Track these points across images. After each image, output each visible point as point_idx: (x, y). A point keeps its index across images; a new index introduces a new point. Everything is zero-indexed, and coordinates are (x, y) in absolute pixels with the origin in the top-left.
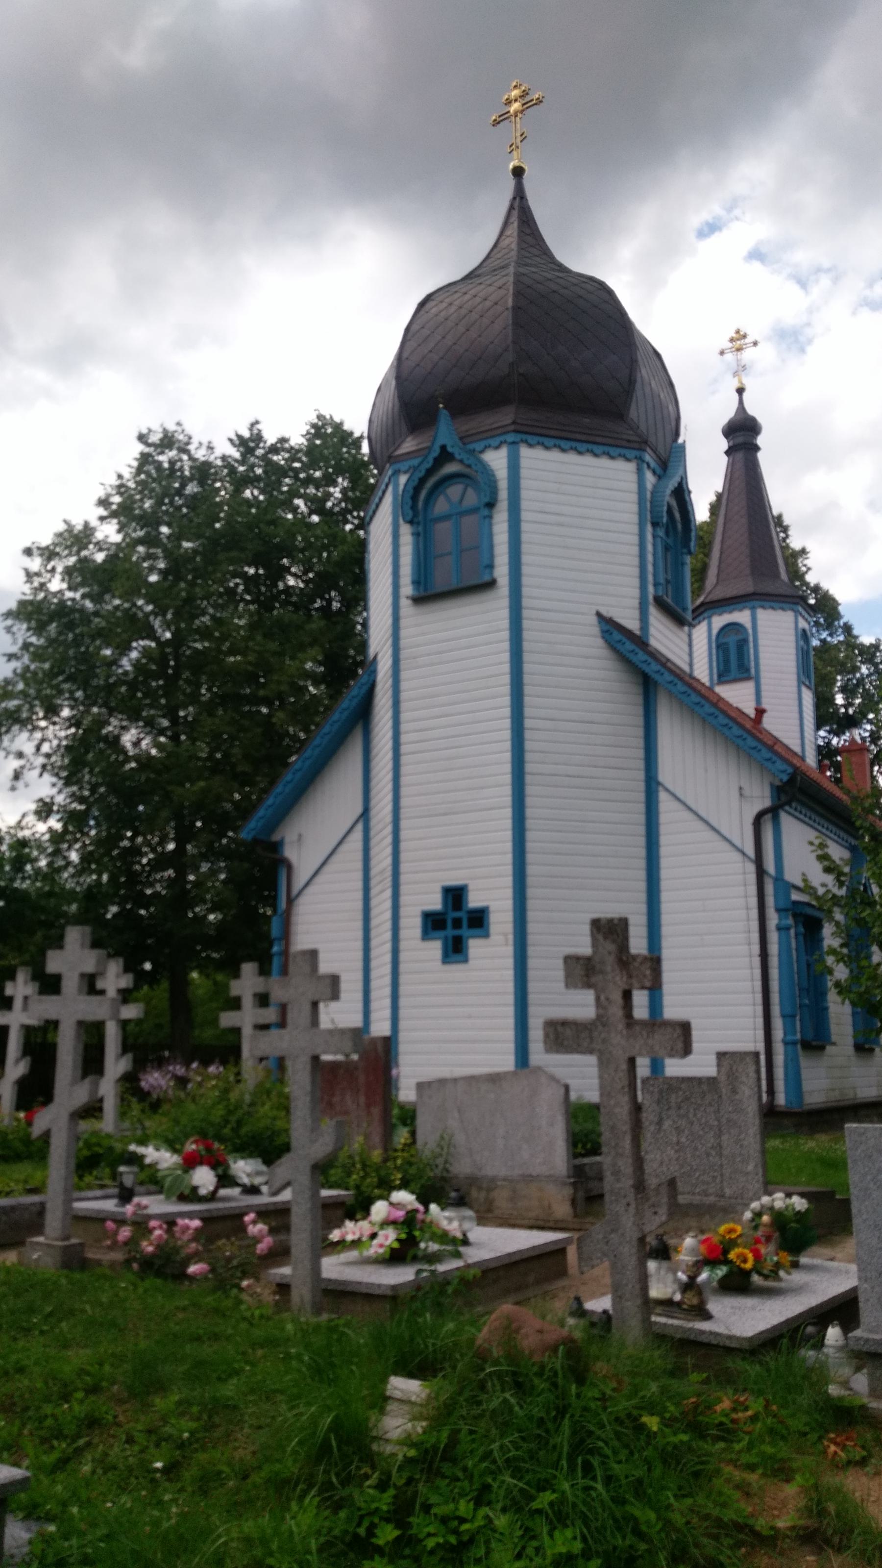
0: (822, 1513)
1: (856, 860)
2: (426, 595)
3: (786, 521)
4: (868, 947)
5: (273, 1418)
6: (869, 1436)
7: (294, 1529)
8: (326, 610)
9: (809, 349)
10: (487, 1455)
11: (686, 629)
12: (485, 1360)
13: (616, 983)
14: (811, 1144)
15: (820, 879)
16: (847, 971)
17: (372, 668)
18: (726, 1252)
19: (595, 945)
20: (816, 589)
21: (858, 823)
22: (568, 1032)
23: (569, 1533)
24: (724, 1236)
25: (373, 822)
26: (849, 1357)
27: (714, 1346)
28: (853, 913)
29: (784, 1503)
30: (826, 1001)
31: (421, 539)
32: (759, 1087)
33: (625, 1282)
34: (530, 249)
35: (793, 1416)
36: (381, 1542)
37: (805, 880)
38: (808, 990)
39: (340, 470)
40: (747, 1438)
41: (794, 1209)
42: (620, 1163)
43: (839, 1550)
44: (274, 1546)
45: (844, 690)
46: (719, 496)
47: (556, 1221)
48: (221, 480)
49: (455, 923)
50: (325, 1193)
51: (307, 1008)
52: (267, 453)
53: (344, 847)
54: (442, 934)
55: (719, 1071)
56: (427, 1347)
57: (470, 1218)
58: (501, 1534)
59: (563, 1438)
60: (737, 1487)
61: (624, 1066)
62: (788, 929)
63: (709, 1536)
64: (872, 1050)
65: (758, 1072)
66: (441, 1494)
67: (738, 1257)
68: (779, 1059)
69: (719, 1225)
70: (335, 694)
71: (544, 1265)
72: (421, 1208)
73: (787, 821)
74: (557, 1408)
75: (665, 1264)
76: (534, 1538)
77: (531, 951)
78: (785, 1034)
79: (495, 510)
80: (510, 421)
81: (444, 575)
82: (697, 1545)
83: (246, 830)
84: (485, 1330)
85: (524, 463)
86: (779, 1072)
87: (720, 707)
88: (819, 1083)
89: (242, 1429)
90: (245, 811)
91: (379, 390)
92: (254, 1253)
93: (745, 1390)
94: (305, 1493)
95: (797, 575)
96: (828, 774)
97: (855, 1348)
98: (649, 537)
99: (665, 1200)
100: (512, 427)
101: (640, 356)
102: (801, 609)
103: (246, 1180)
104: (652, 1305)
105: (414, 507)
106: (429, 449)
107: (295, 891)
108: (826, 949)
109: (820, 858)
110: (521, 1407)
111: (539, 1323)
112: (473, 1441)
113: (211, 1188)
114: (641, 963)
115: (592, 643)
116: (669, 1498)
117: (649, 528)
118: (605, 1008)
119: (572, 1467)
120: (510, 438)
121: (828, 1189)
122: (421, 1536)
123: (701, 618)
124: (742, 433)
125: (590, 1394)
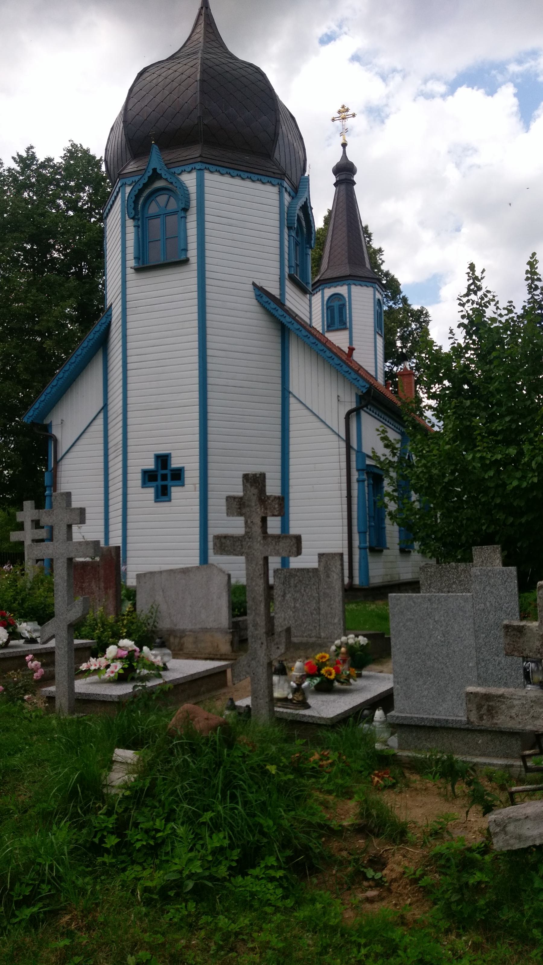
2: (143, 267)
3: (370, 230)
4: (410, 491)
5: (43, 776)
6: (397, 771)
7: (54, 841)
8: (78, 274)
9: (386, 121)
10: (174, 792)
11: (308, 295)
12: (173, 737)
13: (257, 512)
14: (373, 607)
15: (382, 452)
16: (396, 506)
17: (108, 313)
18: (319, 669)
19: (244, 490)
20: (387, 274)
21: (405, 418)
22: (228, 542)
23: (221, 835)
25: (110, 413)
26: (387, 727)
27: (310, 723)
28: (400, 471)
29: (348, 812)
31: (140, 230)
32: (343, 573)
33: (259, 688)
35: (355, 762)
36: (108, 846)
37: (373, 452)
39: (87, 182)
40: (328, 775)
41: (360, 644)
42: (258, 619)
44: (42, 851)
45: (402, 338)
46: (330, 212)
47: (221, 655)
48: (7, 185)
49: (163, 477)
50: (76, 642)
51: (64, 529)
53: (91, 429)
54: (154, 484)
55: (319, 565)
56: (138, 731)
57: (168, 654)
58: (181, 837)
59: (219, 780)
60: (321, 804)
61: (261, 562)
62: (363, 481)
63: (304, 832)
64: (410, 552)
65: (342, 565)
66: (145, 816)
67: (326, 672)
69: (316, 654)
71: (212, 681)
72: (138, 649)
73: (365, 417)
75: (283, 678)
76: (201, 839)
77: (210, 494)
78: (360, 543)
79: (188, 213)
80: (198, 155)
82: (296, 838)
83: (27, 416)
84: (174, 719)
85: (207, 183)
86: (356, 565)
87: (328, 346)
88: (379, 571)
89: (23, 783)
90: (26, 404)
91: (112, 129)
92: (32, 678)
93: (327, 748)
95: (376, 265)
96: (391, 389)
98: (286, 236)
99: (284, 640)
101: (282, 118)
102: (377, 287)
103: (27, 635)
105: (135, 208)
107: (59, 456)
108: (385, 492)
109: (383, 439)
110: (194, 764)
111: (207, 715)
112: (165, 784)
113: (5, 640)
114: (272, 501)
116: (281, 812)
117: (286, 230)
118: (251, 528)
120: (198, 166)
121: (381, 632)
122: (132, 842)
123: (318, 290)
124: (345, 173)
125: (235, 754)
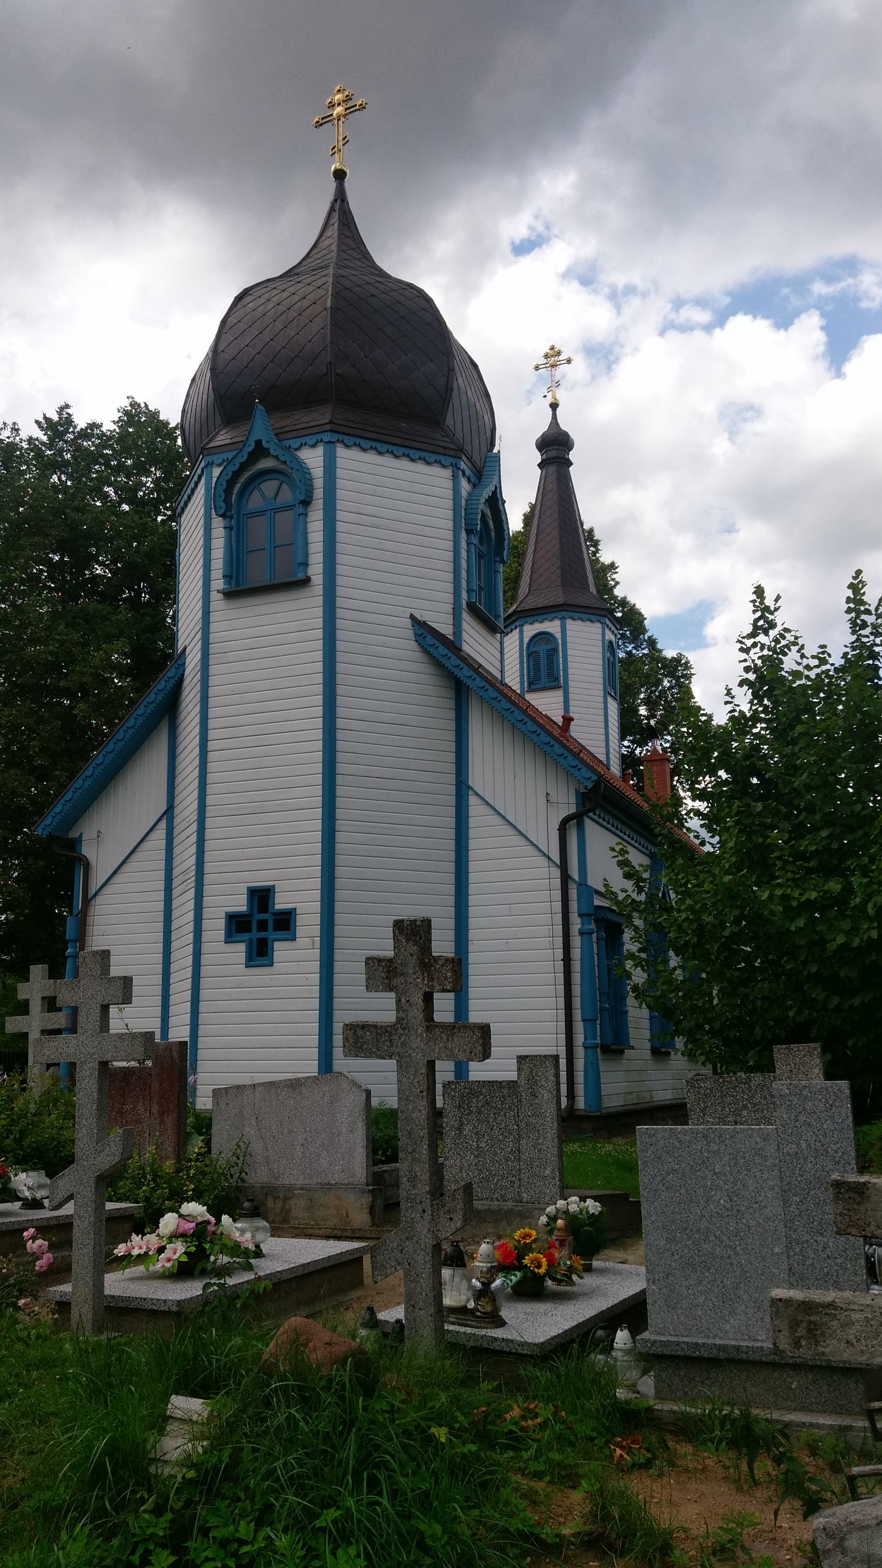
0: (607, 1517)
1: (654, 867)
2: (237, 591)
5: (47, 1442)
7: (61, 1559)
14: (609, 1147)
15: (620, 884)
16: (645, 975)
17: (180, 662)
18: (520, 1257)
20: (624, 603)
23: (352, 1551)
24: (519, 1241)
25: (177, 820)
30: (625, 1005)
31: (234, 533)
32: (558, 1090)
34: (350, 252)
37: (606, 886)
38: (608, 995)
39: (154, 462)
41: (588, 1212)
43: (622, 1554)
45: (647, 702)
46: (533, 507)
47: (353, 1231)
48: (26, 463)
49: (260, 925)
50: (110, 1206)
51: (96, 1012)
52: (76, 438)
53: (145, 846)
54: (246, 936)
56: (211, 1364)
57: (264, 1229)
58: (283, 1555)
59: (349, 1453)
60: (524, 1496)
63: (495, 1547)
65: (557, 1076)
66: (220, 1516)
68: (580, 1064)
70: (141, 688)
71: (339, 1276)
72: (213, 1219)
74: (344, 1423)
75: (459, 1271)
76: (317, 1557)
78: (586, 1039)
79: (310, 508)
80: (327, 421)
81: (258, 571)
83: (42, 826)
84: (272, 1344)
85: (340, 462)
86: (580, 1077)
88: (617, 1087)
89: (12, 1455)
90: (41, 807)
91: (193, 380)
93: (535, 1397)
94: (76, 1520)
95: (606, 589)
97: (643, 1350)
98: (464, 544)
100: (328, 427)
102: (608, 622)
103: (27, 1194)
104: (445, 1313)
105: (227, 501)
106: (244, 442)
107: (92, 891)
108: (625, 953)
109: (621, 864)
110: (307, 1423)
111: (328, 1336)
112: (256, 1459)
115: (407, 646)
116: (455, 1510)
117: (463, 534)
119: (358, 1482)
120: (327, 437)
124: (555, 448)
125: (378, 1407)
